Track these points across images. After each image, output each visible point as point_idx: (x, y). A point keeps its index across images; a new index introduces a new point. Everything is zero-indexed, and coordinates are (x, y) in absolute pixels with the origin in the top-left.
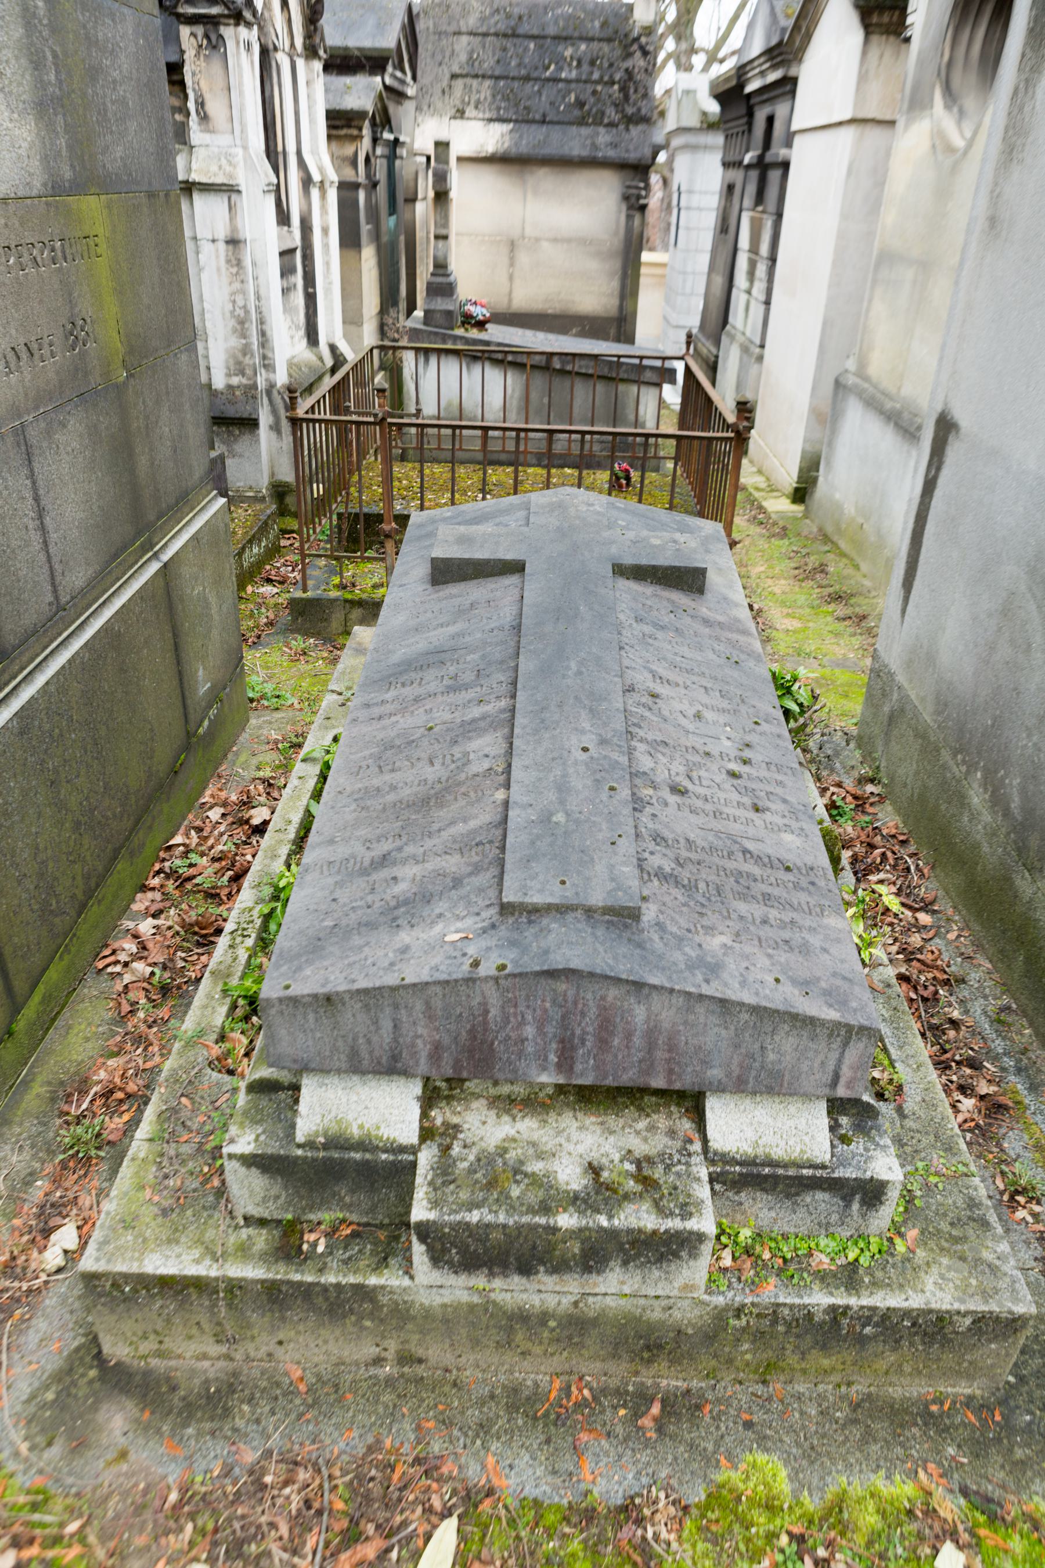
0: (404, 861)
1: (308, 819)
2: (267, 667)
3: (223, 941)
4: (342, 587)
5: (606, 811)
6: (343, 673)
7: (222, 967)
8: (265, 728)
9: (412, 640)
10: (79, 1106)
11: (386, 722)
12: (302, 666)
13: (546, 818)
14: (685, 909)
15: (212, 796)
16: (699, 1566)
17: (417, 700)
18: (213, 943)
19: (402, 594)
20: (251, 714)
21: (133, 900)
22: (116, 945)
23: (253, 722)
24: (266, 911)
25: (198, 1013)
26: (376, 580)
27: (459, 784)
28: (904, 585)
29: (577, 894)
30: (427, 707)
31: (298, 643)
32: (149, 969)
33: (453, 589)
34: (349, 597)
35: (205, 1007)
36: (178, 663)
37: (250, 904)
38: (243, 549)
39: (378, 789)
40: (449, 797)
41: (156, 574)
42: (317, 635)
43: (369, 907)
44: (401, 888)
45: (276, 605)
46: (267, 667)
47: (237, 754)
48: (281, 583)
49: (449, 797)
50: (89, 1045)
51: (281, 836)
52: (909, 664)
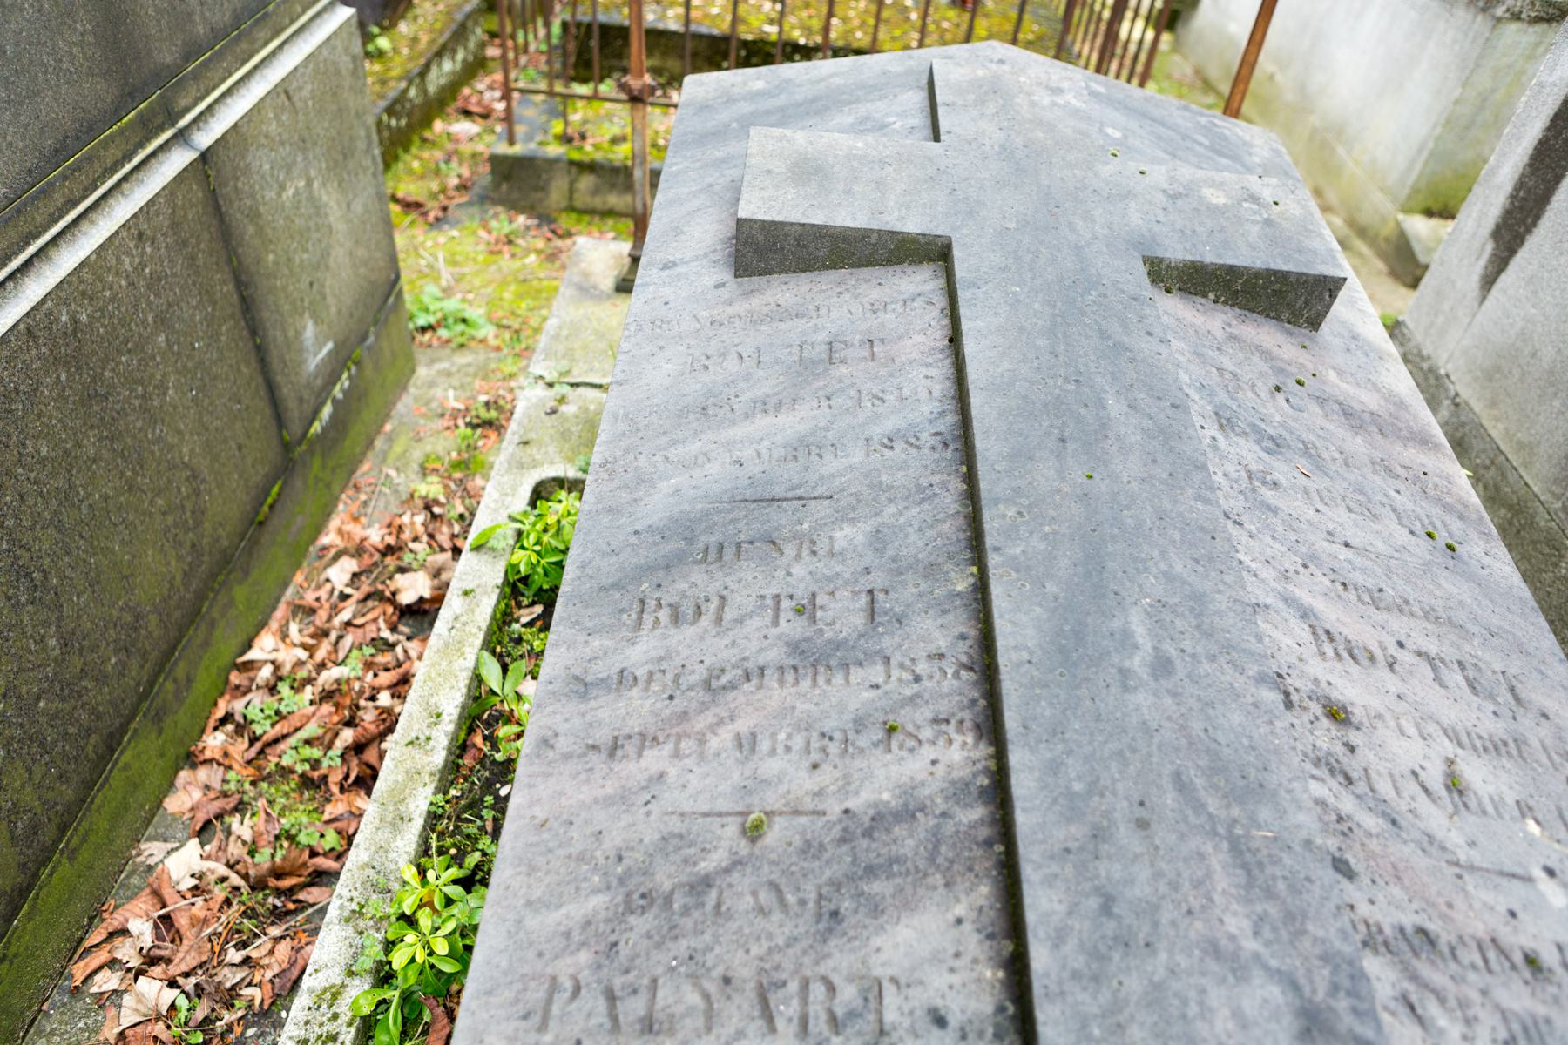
1: (482, 714)
2: (452, 266)
4: (566, 139)
6: (556, 337)
8: (438, 384)
9: (694, 447)
11: (633, 770)
12: (506, 263)
15: (340, 532)
17: (712, 686)
18: (302, 906)
19: (667, 292)
20: (421, 356)
21: (170, 786)
22: (114, 922)
23: (422, 372)
26: (616, 130)
28: (1497, 234)
30: (743, 725)
31: (503, 222)
32: (170, 995)
33: (784, 291)
34: (576, 156)
36: (254, 332)
37: (334, 976)
38: (427, 66)
41: (180, 178)
42: (530, 210)
45: (474, 156)
46: (452, 266)
47: (390, 439)
48: (485, 116)
52: (1490, 376)
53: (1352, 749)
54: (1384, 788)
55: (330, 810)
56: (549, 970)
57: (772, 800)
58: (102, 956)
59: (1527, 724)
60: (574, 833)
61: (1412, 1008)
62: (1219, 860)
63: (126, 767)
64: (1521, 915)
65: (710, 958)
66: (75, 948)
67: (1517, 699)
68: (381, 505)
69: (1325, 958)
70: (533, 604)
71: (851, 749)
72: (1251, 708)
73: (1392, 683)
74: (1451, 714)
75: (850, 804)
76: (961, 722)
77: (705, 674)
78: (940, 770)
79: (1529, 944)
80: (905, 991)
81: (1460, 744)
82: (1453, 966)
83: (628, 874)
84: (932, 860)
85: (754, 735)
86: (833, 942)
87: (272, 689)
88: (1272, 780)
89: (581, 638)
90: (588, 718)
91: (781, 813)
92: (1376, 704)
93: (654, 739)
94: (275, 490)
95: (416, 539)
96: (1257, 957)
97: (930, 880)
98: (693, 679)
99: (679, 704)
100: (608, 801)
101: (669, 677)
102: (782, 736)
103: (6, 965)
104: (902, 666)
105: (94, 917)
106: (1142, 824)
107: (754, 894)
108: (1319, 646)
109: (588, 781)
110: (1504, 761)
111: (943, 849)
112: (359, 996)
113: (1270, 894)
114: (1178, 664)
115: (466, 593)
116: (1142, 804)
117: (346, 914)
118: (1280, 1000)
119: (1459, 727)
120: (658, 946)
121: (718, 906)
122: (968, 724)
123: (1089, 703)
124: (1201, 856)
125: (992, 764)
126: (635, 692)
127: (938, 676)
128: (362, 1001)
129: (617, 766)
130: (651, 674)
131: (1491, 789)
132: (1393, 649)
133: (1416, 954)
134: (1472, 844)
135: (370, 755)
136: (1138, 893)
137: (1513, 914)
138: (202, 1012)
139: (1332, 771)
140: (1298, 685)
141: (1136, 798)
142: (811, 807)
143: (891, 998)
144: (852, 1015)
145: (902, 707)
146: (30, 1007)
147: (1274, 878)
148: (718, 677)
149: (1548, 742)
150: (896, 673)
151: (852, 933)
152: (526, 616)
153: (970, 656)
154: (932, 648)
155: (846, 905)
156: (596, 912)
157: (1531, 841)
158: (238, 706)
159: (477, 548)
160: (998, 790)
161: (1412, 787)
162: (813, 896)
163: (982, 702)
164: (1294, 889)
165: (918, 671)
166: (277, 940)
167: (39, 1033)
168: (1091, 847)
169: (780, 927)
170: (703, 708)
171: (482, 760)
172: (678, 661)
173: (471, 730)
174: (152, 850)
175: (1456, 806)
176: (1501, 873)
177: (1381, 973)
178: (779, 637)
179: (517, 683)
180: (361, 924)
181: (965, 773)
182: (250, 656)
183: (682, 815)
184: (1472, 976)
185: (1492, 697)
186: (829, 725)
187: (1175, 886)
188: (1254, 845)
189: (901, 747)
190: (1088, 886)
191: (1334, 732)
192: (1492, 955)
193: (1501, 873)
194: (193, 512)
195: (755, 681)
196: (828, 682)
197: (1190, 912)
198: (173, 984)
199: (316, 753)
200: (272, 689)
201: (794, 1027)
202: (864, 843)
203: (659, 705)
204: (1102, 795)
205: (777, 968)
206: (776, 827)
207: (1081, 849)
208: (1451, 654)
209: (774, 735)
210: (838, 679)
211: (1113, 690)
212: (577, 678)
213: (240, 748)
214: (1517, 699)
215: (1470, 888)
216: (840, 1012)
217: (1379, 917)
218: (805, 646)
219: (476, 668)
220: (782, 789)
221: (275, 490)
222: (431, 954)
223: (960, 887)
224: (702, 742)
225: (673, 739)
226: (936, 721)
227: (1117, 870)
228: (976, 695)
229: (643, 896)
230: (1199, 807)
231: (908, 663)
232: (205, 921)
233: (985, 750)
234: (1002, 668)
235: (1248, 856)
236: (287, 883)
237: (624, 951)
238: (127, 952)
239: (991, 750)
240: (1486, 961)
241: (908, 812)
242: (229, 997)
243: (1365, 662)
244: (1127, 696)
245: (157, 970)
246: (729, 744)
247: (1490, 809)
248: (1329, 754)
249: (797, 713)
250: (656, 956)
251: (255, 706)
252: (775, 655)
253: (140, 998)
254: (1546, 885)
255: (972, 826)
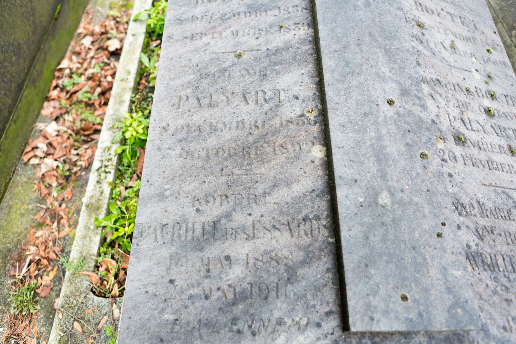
0: (234, 234)
1: (143, 74)
3: (93, 177)
5: (425, 189)
7: (93, 201)
10: (20, 272)
11: (199, 43)
13: (373, 197)
14: (496, 298)
15: (84, 28)
16: (195, 1)
17: (223, 18)
18: (93, 140)
21: (42, 107)
22: (33, 145)
24: (120, 151)
25: (80, 243)
27: (276, 132)
29: (420, 315)
30: (234, 29)
32: (55, 164)
35: (84, 237)
37: (108, 144)
39: (199, 129)
40: (269, 149)
43: (207, 298)
44: (236, 273)
49: (269, 149)
50: (24, 220)
51: (124, 84)
53: (424, 35)
54: (432, 45)
55: (97, 113)
56: (178, 94)
57: (244, 48)
58: (31, 154)
59: (477, 35)
60: (182, 60)
61: (433, 97)
62: (381, 54)
63: (26, 97)
64: (466, 79)
65: (228, 88)
66: (22, 152)
67: (476, 28)
68: (97, 19)
69: (409, 78)
70: (156, 40)
71: (268, 33)
72: (394, 16)
73: (438, 19)
74: (454, 29)
75: (269, 47)
76: (303, 24)
77: (220, 16)
78: (297, 36)
79: (467, 86)
80: (286, 92)
81: (456, 37)
82: (445, 89)
83: (200, 69)
84: (294, 59)
85: (237, 31)
86: (264, 82)
87: (71, 77)
88: (398, 35)
89: (178, 8)
90: (183, 30)
91: (247, 51)
92: (432, 24)
93: (206, 34)
94: (59, 7)
95: (112, 29)
96: (390, 77)
97: (294, 65)
98: (216, 17)
99: (212, 24)
100: (192, 51)
101: (208, 17)
102: (246, 31)
103: (2, 152)
104: (284, 10)
105: (27, 144)
106: (359, 45)
107: (240, 72)
108: (417, 7)
109: (185, 46)
110: (469, 43)
111: (298, 57)
112: (117, 149)
113: (395, 62)
114: (373, 4)
115: (133, 35)
116: (359, 40)
117: (109, 128)
118: (396, 87)
119: (457, 33)
120: (211, 86)
121: (229, 75)
122: (305, 24)
123: (344, 14)
124: (376, 53)
125: (313, 34)
126: (198, 22)
127: (296, 12)
128: (117, 150)
129: (194, 42)
130: (202, 16)
131: (464, 49)
132: (440, 10)
133: (435, 85)
134: (456, 62)
135: (107, 95)
136: (356, 62)
137: (464, 79)
138: (67, 167)
139: (417, 40)
140: (409, 16)
141: (357, 38)
142: (256, 49)
143: (282, 94)
144: (271, 98)
145: (285, 20)
146: (12, 167)
147: (397, 59)
148: (225, 16)
149: (483, 40)
150: (282, 12)
151: (270, 79)
152: (154, 44)
153: (306, 6)
154: (294, 4)
155: (268, 72)
156: (191, 79)
157: (473, 63)
158: (60, 82)
159: (135, 20)
160: (316, 40)
161: (440, 46)
162: (258, 71)
163: (310, 18)
164: (402, 61)
165: (289, 11)
166: (87, 149)
167: (17, 175)
168: (343, 50)
169: (248, 79)
170: (220, 25)
171: (146, 87)
172: (211, 12)
173: (141, 79)
174: (40, 126)
175: (452, 52)
176: (463, 69)
177: (426, 88)
178: (244, 4)
179: (154, 63)
180: (114, 130)
181: (305, 37)
182: (60, 66)
183: (216, 53)
184: (450, 91)
185: (468, 26)
186: (261, 27)
187: (367, 60)
188: (391, 51)
189: (284, 31)
190: (341, 60)
191: (419, 30)
192: (457, 87)
193: (463, 69)
194: (31, 9)
195: (236, 17)
196: (261, 15)
197: (371, 66)
198: (56, 160)
199: (89, 95)
200: (71, 77)
201: (254, 102)
202: (273, 57)
203: (206, 25)
204: (347, 37)
205: (248, 89)
206: (246, 55)
207: (340, 50)
208: (457, 13)
209: (244, 31)
210: (264, 14)
211: (352, 10)
212: (178, 19)
213: (63, 95)
214: (476, 28)
215: (453, 72)
216: (267, 98)
217: (426, 75)
218: (252, 6)
219: (140, 58)
220: (247, 45)
221: (59, 7)
222: (137, 133)
223: (303, 66)
224: (221, 34)
225: (211, 34)
226: (295, 24)
227: (350, 56)
228: (308, 16)
229: (205, 74)
230: (376, 41)
231: (286, 9)
232: (62, 143)
233: (311, 31)
234: (317, 4)
235: (390, 53)
236: (87, 133)
237: (201, 88)
238: (39, 153)
239: (313, 30)
240: (455, 89)
241: (287, 48)
242: (75, 164)
243: (431, 13)
244: (356, 12)
245: (50, 157)
246: (229, 34)
247: (462, 54)
248: (416, 35)
249: (251, 24)
250: (211, 89)
251: (65, 81)
252: (242, 9)
253: (46, 165)
254: (475, 74)
255: (307, 50)
